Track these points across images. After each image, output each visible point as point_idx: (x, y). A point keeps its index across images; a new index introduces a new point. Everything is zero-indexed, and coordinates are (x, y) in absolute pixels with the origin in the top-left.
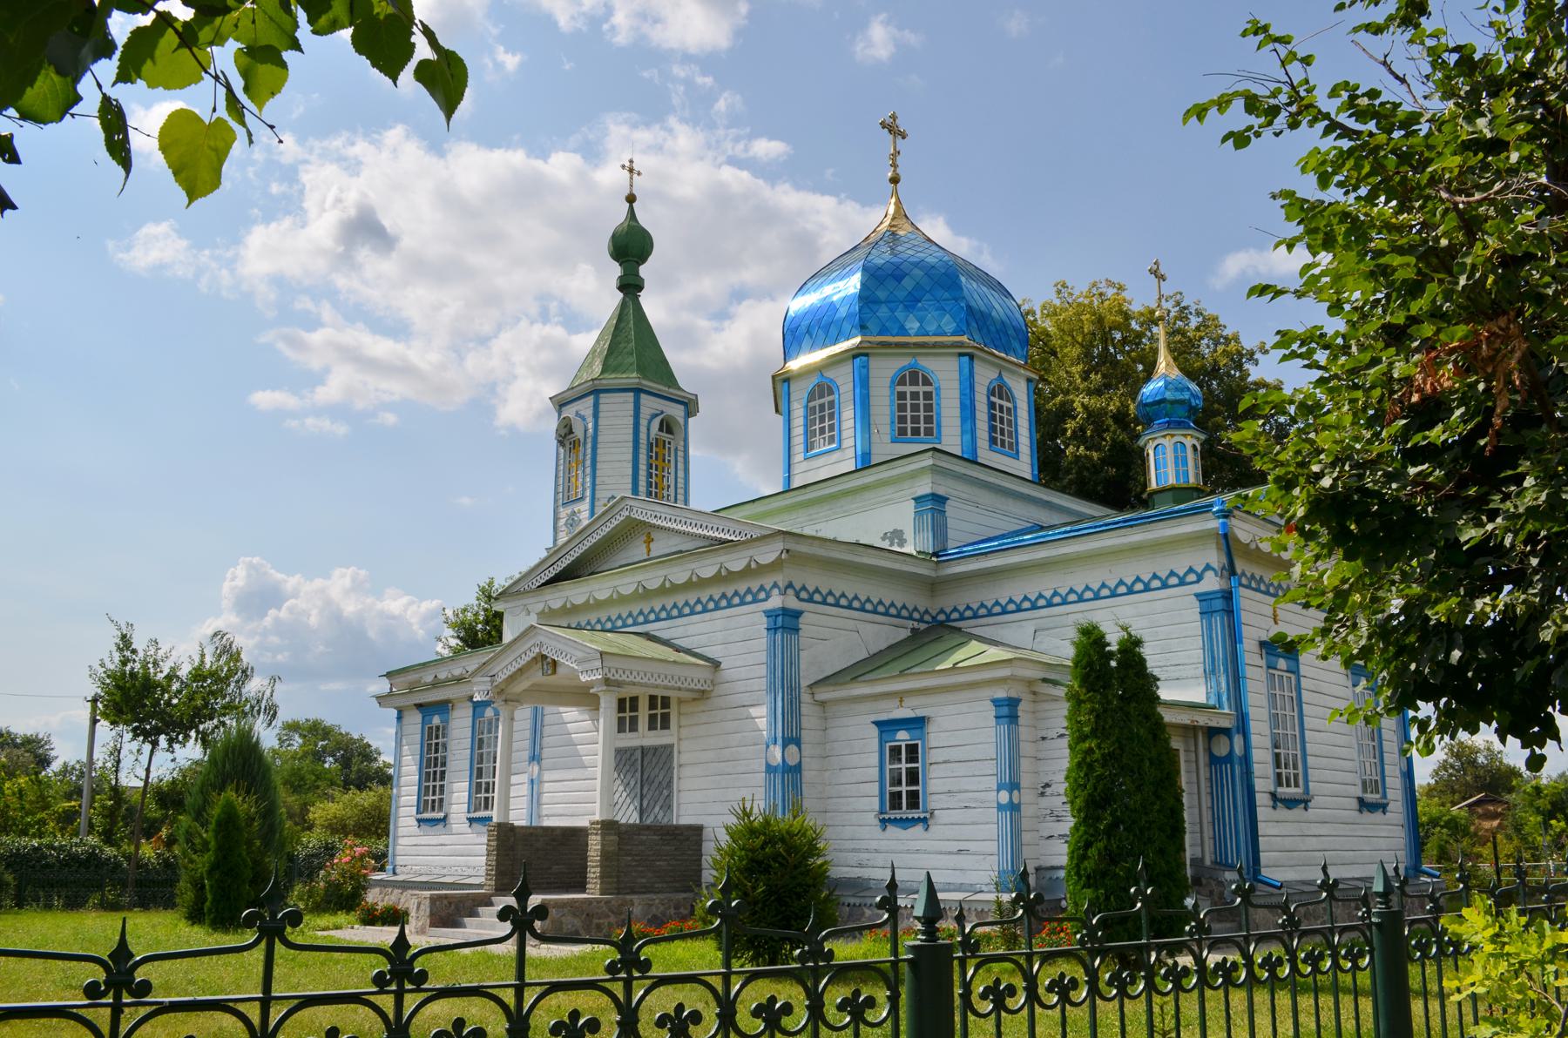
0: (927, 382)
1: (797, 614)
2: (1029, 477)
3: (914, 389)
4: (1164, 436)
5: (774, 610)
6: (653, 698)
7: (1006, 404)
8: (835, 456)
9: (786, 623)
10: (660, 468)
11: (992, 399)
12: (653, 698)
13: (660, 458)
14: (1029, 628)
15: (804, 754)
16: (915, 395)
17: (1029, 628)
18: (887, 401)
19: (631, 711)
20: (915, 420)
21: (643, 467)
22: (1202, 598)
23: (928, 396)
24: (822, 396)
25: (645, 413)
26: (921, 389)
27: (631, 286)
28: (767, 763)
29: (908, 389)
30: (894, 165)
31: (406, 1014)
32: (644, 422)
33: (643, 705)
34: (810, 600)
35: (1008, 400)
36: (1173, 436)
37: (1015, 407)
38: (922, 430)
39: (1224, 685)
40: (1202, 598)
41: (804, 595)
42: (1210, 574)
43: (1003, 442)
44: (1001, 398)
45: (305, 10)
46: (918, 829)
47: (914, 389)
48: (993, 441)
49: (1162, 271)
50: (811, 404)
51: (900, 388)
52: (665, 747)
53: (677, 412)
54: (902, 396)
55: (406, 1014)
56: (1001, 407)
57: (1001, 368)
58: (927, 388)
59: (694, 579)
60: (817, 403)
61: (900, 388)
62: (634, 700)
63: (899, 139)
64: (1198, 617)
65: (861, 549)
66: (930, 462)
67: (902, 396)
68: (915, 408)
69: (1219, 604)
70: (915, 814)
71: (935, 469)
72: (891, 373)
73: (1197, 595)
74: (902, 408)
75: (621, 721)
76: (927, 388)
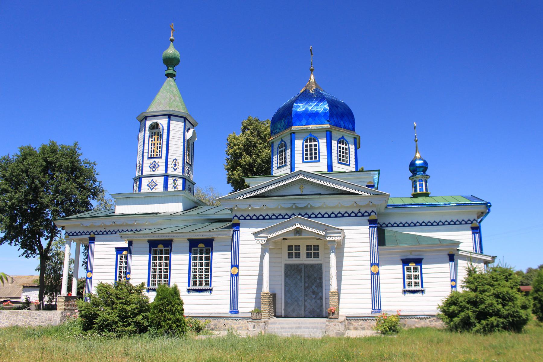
3: (311, 143)
6: (309, 247)
7: (345, 146)
8: (285, 168)
11: (339, 145)
12: (309, 247)
20: (311, 154)
28: (371, 272)
29: (309, 144)
35: (346, 145)
39: (429, 254)
43: (343, 160)
44: (343, 144)
45: (162, 53)
46: (207, 293)
47: (311, 143)
52: (318, 265)
54: (306, 146)
56: (343, 148)
59: (294, 207)
62: (298, 247)
70: (208, 287)
75: (289, 254)
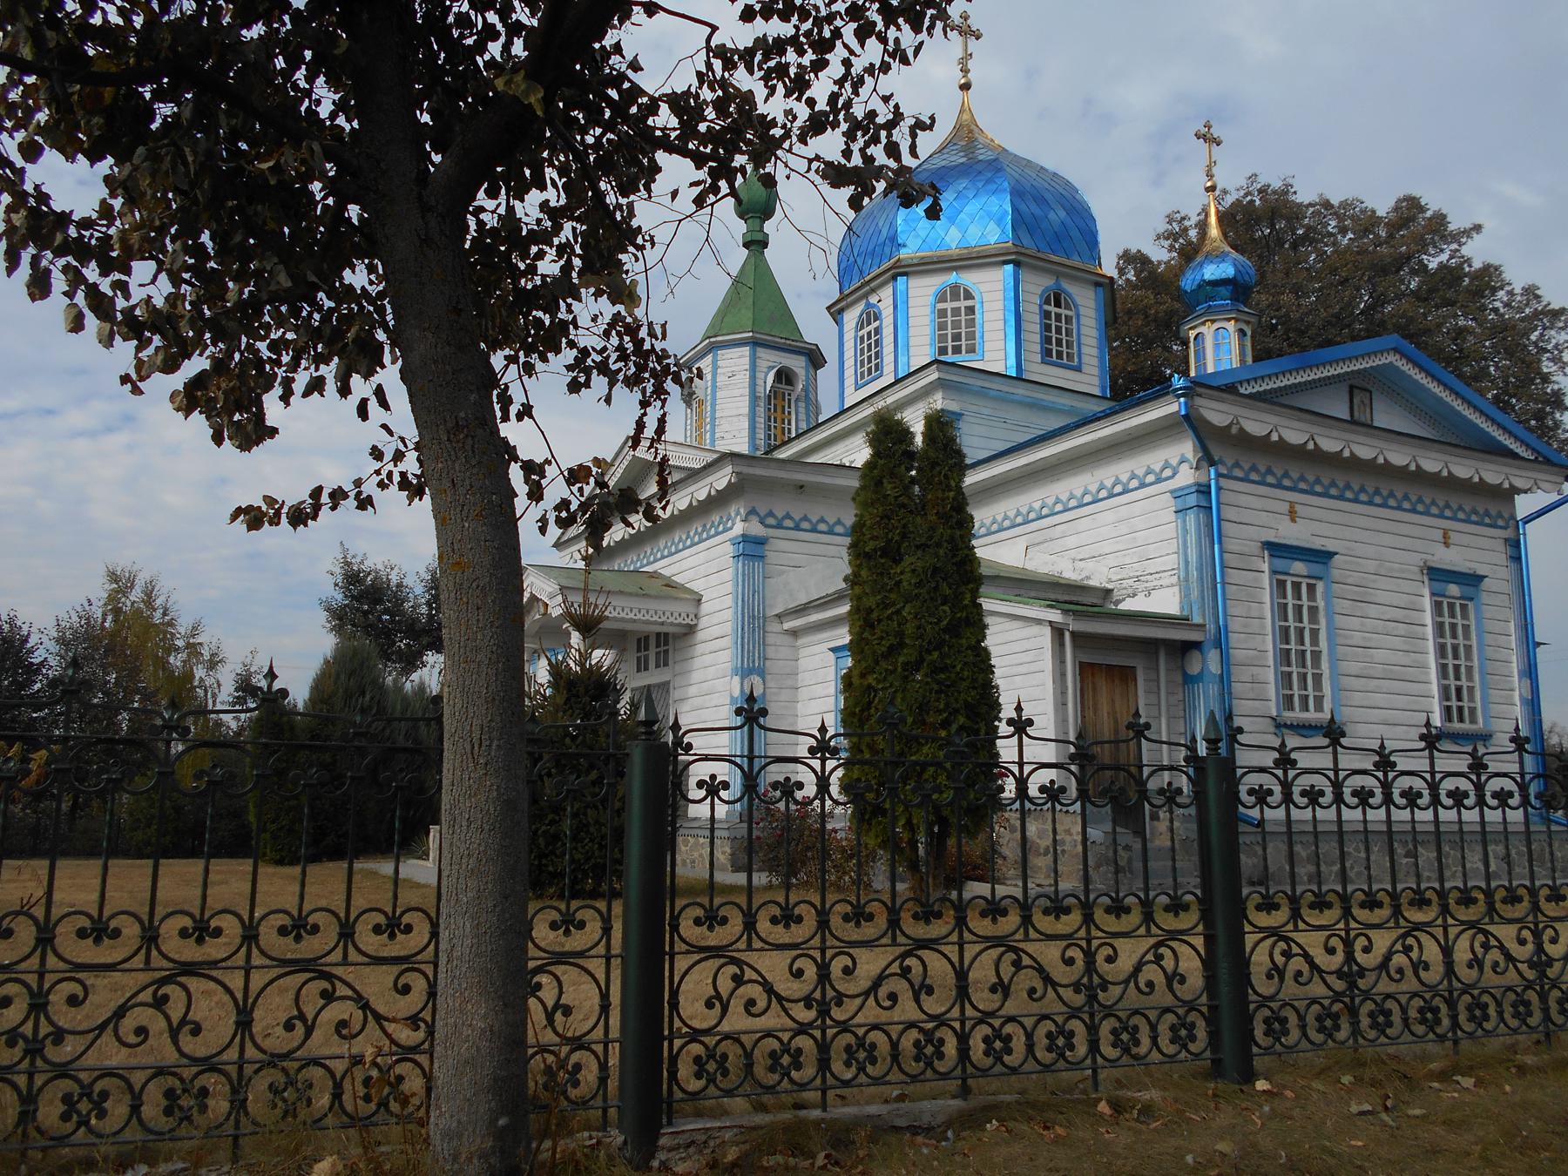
0: (969, 296)
1: (761, 542)
2: (1097, 392)
3: (955, 304)
4: (1203, 323)
5: (737, 537)
9: (752, 549)
10: (779, 420)
11: (1046, 307)
13: (779, 409)
14: (1022, 543)
15: (768, 685)
16: (956, 312)
17: (1022, 543)
18: (927, 320)
19: (1288, 651)
21: (761, 420)
22: (1177, 494)
23: (971, 310)
24: (869, 324)
25: (763, 365)
26: (963, 304)
27: (756, 244)
29: (949, 305)
30: (965, 71)
31: (244, 949)
32: (760, 375)
33: (652, 642)
34: (779, 526)
35: (1068, 307)
36: (1213, 321)
37: (1078, 316)
38: (963, 348)
40: (1177, 494)
41: (771, 521)
42: (1185, 467)
48: (1047, 353)
49: (1215, 132)
50: (860, 334)
51: (941, 306)
53: (798, 364)
54: (943, 313)
55: (244, 949)
57: (1058, 275)
58: (969, 303)
60: (864, 332)
61: (941, 306)
63: (972, 42)
64: (1173, 517)
65: (833, 470)
66: (935, 376)
67: (943, 313)
68: (956, 325)
69: (1192, 500)
71: (940, 384)
72: (932, 290)
73: (1171, 492)
74: (942, 327)
76: (969, 303)
